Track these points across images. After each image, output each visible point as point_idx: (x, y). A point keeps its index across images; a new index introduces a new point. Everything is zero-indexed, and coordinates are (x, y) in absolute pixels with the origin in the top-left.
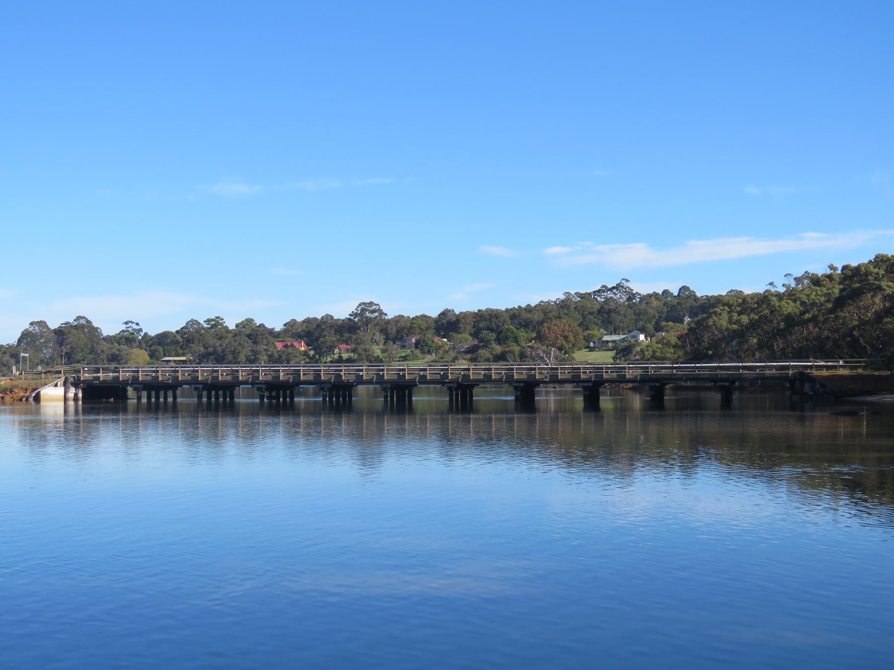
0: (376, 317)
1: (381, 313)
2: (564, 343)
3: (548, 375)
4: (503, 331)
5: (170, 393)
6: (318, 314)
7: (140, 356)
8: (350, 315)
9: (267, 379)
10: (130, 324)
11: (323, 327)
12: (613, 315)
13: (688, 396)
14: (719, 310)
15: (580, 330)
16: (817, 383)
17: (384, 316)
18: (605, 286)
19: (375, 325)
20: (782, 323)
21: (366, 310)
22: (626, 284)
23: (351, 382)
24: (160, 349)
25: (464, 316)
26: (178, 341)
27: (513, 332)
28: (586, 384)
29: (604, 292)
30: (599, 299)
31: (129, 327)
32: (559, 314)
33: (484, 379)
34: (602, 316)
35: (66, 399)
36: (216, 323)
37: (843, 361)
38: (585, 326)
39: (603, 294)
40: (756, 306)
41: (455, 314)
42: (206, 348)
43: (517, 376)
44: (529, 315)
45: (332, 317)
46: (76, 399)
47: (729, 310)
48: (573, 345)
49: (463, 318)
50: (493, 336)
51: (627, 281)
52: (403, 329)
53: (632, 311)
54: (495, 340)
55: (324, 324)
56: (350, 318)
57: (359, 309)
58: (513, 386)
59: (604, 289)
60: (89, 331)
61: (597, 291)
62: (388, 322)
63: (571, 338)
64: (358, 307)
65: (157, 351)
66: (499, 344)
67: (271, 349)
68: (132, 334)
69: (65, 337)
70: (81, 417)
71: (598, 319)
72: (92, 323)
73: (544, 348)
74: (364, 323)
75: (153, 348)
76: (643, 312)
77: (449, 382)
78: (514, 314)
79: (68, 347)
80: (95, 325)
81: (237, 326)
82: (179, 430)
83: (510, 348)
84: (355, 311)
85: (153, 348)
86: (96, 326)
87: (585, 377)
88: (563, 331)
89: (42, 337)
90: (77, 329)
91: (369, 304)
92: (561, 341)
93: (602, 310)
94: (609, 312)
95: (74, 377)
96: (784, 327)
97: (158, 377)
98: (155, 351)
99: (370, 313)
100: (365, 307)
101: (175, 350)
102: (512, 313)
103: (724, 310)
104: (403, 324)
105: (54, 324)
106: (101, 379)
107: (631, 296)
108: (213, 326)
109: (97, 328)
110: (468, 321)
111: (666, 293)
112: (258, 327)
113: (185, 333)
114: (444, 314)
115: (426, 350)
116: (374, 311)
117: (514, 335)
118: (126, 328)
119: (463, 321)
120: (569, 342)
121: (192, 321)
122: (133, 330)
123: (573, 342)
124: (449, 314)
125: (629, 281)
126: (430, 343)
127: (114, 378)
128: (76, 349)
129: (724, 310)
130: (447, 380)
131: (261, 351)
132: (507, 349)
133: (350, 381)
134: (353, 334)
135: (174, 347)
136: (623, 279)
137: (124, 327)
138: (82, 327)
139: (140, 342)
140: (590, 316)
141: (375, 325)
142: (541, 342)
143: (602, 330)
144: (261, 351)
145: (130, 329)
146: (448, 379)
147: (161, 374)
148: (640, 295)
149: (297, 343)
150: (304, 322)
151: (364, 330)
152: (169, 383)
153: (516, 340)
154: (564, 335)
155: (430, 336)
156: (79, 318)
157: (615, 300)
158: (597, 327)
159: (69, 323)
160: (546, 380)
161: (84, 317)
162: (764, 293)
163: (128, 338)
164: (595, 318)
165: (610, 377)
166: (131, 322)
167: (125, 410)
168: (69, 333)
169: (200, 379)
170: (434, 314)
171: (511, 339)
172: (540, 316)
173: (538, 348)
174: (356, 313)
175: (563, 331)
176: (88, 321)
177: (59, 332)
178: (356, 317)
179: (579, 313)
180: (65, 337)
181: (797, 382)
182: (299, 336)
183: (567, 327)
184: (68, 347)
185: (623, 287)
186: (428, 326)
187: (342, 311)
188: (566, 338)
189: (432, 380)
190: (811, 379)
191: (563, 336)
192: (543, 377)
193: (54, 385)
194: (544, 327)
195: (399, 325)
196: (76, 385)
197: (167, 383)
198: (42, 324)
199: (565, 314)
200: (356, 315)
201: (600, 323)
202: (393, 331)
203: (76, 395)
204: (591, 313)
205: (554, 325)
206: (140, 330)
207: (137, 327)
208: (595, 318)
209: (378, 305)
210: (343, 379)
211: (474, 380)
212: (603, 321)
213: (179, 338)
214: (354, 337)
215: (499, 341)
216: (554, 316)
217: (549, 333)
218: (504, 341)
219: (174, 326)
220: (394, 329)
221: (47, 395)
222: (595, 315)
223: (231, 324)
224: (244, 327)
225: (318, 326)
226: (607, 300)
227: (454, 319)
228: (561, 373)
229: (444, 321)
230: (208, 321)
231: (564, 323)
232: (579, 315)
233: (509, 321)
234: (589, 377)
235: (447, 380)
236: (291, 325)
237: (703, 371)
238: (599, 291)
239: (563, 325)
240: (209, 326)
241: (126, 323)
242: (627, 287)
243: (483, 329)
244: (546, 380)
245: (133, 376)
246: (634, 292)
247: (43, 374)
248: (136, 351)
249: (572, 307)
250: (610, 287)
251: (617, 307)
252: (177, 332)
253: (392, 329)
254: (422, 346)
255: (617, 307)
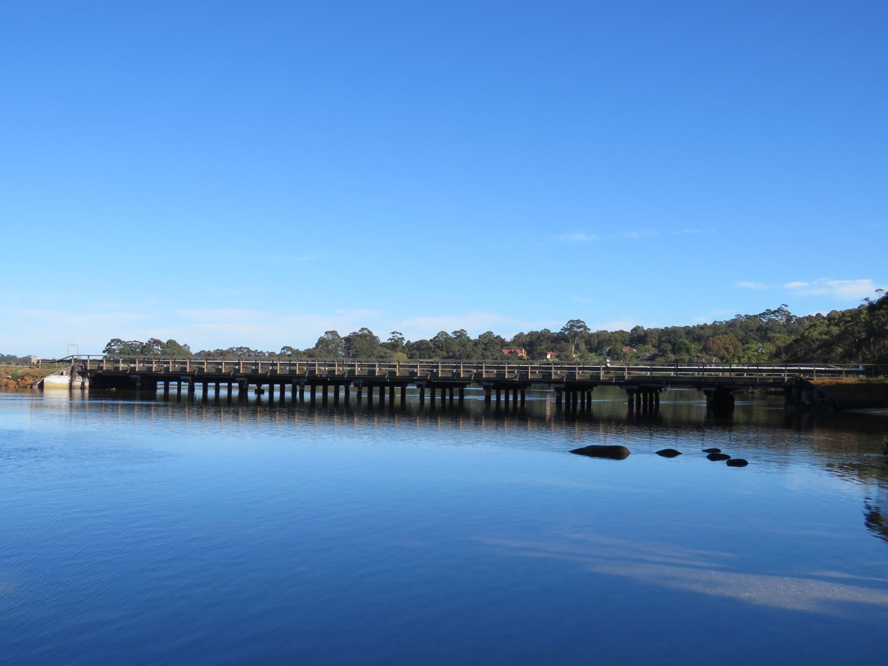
0: (581, 332)
1: (586, 328)
2: (725, 353)
3: (518, 374)
4: (678, 344)
5: (342, 388)
6: (538, 328)
7: (401, 358)
8: (562, 330)
9: (247, 372)
10: (396, 334)
11: (542, 338)
12: (768, 332)
13: (140, 403)
14: (818, 323)
15: (739, 344)
16: (815, 390)
17: (587, 331)
18: (769, 310)
19: (581, 338)
20: (863, 334)
21: (574, 326)
22: (785, 308)
23: (323, 377)
24: (417, 353)
25: (651, 332)
26: (430, 347)
27: (685, 344)
28: (558, 386)
29: (768, 314)
30: (763, 320)
31: (395, 336)
32: (726, 331)
33: (452, 377)
34: (760, 333)
35: (71, 387)
36: (461, 335)
37: (862, 366)
38: (744, 341)
39: (767, 316)
40: (850, 319)
41: (644, 330)
42: (448, 353)
43: (486, 375)
44: (701, 332)
45: (549, 331)
46: (83, 388)
47: (828, 323)
48: (733, 355)
49: (650, 333)
50: (669, 347)
51: (786, 306)
52: (603, 341)
53: (786, 330)
54: (670, 351)
55: (543, 336)
56: (561, 332)
57: (569, 325)
58: (483, 385)
59: (769, 312)
60: (370, 340)
61: (762, 314)
62: (592, 335)
63: (732, 350)
64: (568, 323)
65: (415, 355)
66: (674, 354)
67: (496, 355)
68: (397, 341)
69: (351, 343)
70: (87, 402)
71: (757, 335)
72: (372, 333)
73: (708, 357)
74: (572, 336)
75: (412, 352)
76: (795, 330)
77: (418, 380)
78: (689, 330)
79: (354, 350)
80: (375, 334)
81: (480, 337)
82: (136, 419)
83: (682, 357)
84: (566, 327)
85: (412, 352)
86: (375, 335)
87: (557, 377)
88: (725, 344)
89: (334, 343)
90: (361, 338)
91: (577, 321)
92: (723, 352)
93: (760, 328)
94: (766, 330)
95: (82, 367)
96: (865, 337)
97: (460, 374)
98: (413, 354)
99: (577, 328)
100: (573, 324)
101: (429, 354)
102: (687, 330)
103: (823, 323)
104: (603, 337)
105: (344, 333)
106: (104, 369)
107: (789, 318)
108: (458, 337)
109: (376, 337)
110: (654, 336)
111: (819, 316)
112: (495, 338)
113: (436, 341)
114: (635, 330)
115: (616, 358)
116: (580, 327)
117: (686, 347)
118: (393, 337)
119: (650, 335)
120: (730, 353)
121: (442, 332)
122: (398, 338)
123: (733, 353)
124: (639, 330)
125: (787, 306)
126: (619, 352)
127: (329, 371)
128: (360, 351)
129: (823, 323)
130: (416, 378)
131: (488, 356)
132: (678, 358)
133: (323, 376)
134: (558, 344)
135: (427, 352)
136: (783, 305)
137: (391, 336)
138: (365, 336)
139: (404, 348)
140: (751, 333)
141: (581, 338)
142: (706, 352)
143: (760, 344)
144: (488, 356)
145: (396, 338)
146: (417, 376)
147: (463, 371)
148: (796, 317)
149: (519, 350)
150: (529, 334)
151: (572, 341)
152: (161, 374)
153: (688, 351)
154: (725, 347)
155: (619, 346)
156: (363, 329)
157: (777, 321)
158: (755, 342)
159: (356, 333)
160: (515, 379)
161: (366, 329)
162: (859, 307)
163: (394, 345)
164: (754, 334)
165: (583, 378)
166: (397, 332)
167: (153, 397)
168: (354, 340)
169: (188, 371)
170: (628, 329)
171: (683, 350)
172: (710, 333)
173: (703, 357)
174: (566, 328)
175: (725, 344)
176: (369, 332)
177: (348, 340)
178: (566, 331)
179: (743, 331)
180: (351, 343)
181: (794, 389)
182: (524, 345)
183: (728, 341)
184: (354, 350)
185: (782, 310)
186: (625, 339)
187: (556, 326)
188: (727, 349)
189: (174, 373)
190: (811, 387)
191: (725, 348)
192: (513, 377)
193: (60, 373)
194: (709, 341)
195: (600, 338)
196: (83, 374)
197: (159, 374)
198: (334, 333)
199: (731, 331)
200: (566, 329)
201: (758, 338)
202: (595, 342)
203: (83, 383)
204: (752, 331)
205: (718, 339)
206: (403, 339)
207: (401, 337)
208: (754, 334)
209: (583, 322)
210: (317, 373)
211: (464, 379)
212: (761, 337)
213: (431, 345)
214: (558, 346)
215: (674, 351)
216: (721, 332)
217: (713, 346)
218: (678, 351)
219: (428, 336)
220: (596, 341)
221: (51, 383)
222: (755, 332)
223: (473, 336)
224: (485, 338)
225: (538, 338)
226: (770, 320)
227: (643, 334)
228: (508, 372)
229: (635, 336)
230: (455, 332)
231: (726, 338)
232: (742, 332)
233: (685, 336)
234: (561, 377)
235: (416, 378)
236: (519, 337)
237: (775, 375)
238: (763, 314)
239: (724, 339)
240: (455, 336)
241: (393, 333)
242: (787, 311)
243: (664, 342)
244: (515, 379)
245: (349, 372)
246: (792, 315)
247: (56, 363)
248: (400, 354)
249: (738, 325)
250: (773, 310)
251: (773, 326)
252: (431, 340)
253: (594, 341)
254: (613, 354)
255: (773, 326)
